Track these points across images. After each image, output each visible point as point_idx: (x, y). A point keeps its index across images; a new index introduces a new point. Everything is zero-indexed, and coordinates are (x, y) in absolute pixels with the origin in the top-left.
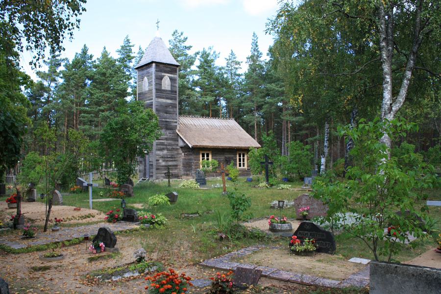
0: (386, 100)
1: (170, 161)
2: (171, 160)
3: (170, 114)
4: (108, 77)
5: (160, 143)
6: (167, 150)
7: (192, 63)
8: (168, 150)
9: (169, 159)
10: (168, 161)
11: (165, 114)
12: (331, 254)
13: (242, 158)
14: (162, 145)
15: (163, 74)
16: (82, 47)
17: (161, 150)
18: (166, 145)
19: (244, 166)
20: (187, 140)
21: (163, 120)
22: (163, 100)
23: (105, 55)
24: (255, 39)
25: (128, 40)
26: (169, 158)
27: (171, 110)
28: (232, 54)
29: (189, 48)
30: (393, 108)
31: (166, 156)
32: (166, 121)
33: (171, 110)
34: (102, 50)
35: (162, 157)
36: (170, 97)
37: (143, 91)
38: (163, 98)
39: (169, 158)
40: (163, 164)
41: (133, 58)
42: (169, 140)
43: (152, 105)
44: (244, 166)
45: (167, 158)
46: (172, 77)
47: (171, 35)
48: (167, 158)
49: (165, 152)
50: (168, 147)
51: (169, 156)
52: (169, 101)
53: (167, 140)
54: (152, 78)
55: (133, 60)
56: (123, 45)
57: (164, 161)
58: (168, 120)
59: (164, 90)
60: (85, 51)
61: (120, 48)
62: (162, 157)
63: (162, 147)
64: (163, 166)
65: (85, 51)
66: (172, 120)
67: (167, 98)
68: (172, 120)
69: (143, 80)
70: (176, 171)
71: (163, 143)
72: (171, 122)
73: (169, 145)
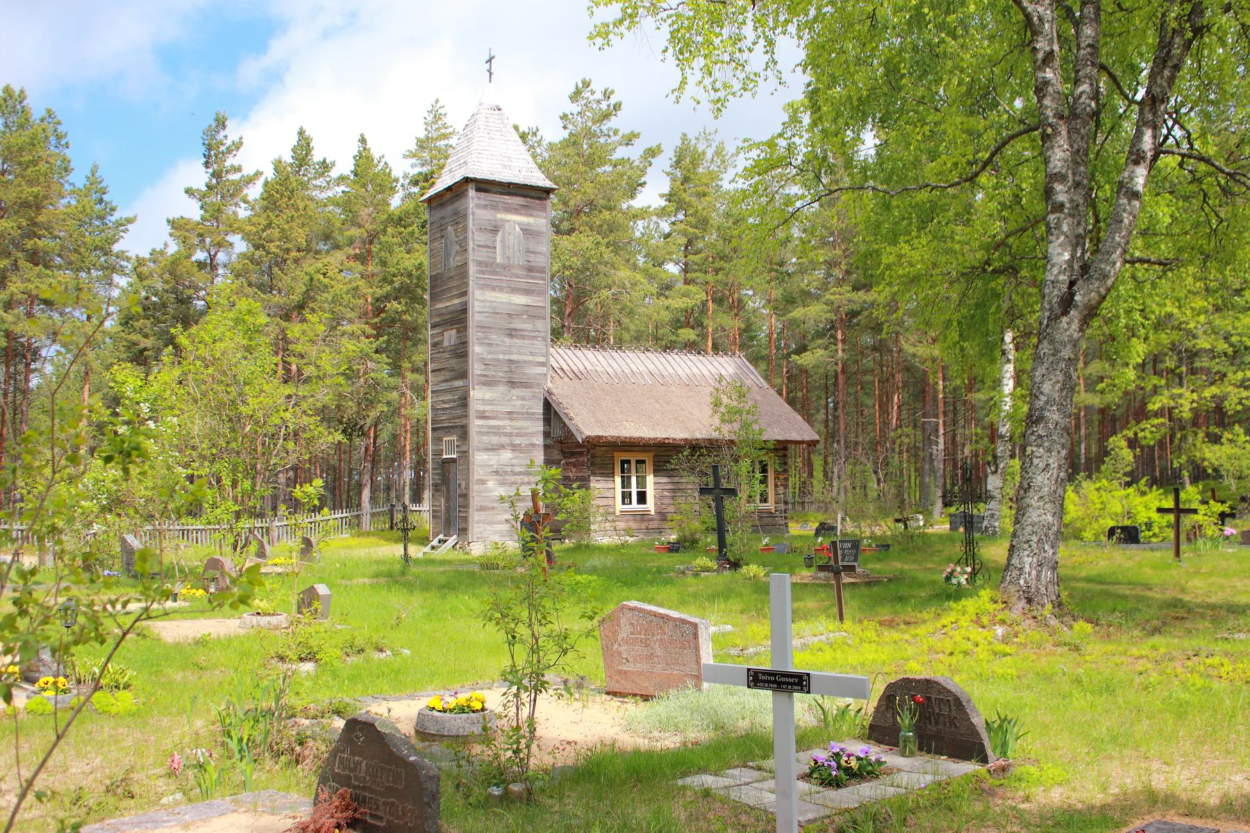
0: (1055, 270)
2: (526, 479)
3: (523, 337)
5: (490, 427)
7: (634, 188)
8: (515, 448)
11: (507, 340)
14: (495, 434)
15: (501, 216)
16: (294, 140)
17: (493, 449)
18: (511, 435)
21: (501, 357)
22: (499, 295)
23: (364, 160)
25: (437, 118)
26: (520, 473)
27: (528, 326)
29: (629, 140)
30: (1077, 298)
32: (511, 361)
33: (528, 326)
34: (354, 149)
35: (497, 472)
36: (523, 286)
38: (501, 289)
42: (515, 419)
45: (514, 473)
46: (528, 224)
47: (49, 107)
48: (514, 473)
49: (507, 455)
51: (517, 469)
52: (521, 300)
56: (422, 135)
57: (503, 483)
58: (514, 357)
60: (304, 146)
61: (413, 147)
62: (497, 472)
63: (495, 440)
65: (304, 146)
67: (514, 290)
71: (499, 427)
72: (525, 362)
73: (519, 435)
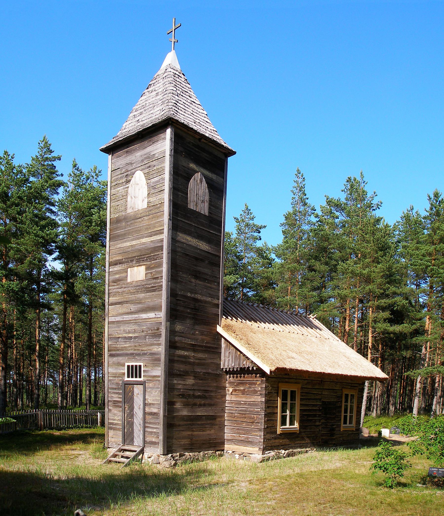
1: (200, 405)
3: (205, 280)
4: (13, 204)
6: (195, 377)
8: (196, 376)
9: (198, 401)
10: (195, 404)
12: (49, 450)
13: (289, 402)
18: (193, 364)
19: (351, 423)
20: (257, 352)
21: (189, 295)
22: (189, 238)
24: (300, 180)
26: (199, 397)
27: (206, 271)
28: (247, 211)
31: (191, 393)
37: (129, 211)
39: (199, 397)
40: (185, 413)
41: (60, 184)
43: (161, 248)
44: (351, 423)
50: (198, 370)
53: (194, 351)
54: (161, 172)
55: (61, 190)
57: (186, 405)
58: (199, 297)
59: (194, 212)
64: (183, 418)
66: (209, 299)
67: (200, 237)
68: (209, 299)
69: (128, 182)
70: (213, 431)
72: (206, 302)
